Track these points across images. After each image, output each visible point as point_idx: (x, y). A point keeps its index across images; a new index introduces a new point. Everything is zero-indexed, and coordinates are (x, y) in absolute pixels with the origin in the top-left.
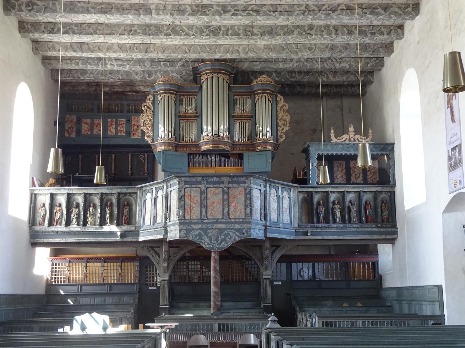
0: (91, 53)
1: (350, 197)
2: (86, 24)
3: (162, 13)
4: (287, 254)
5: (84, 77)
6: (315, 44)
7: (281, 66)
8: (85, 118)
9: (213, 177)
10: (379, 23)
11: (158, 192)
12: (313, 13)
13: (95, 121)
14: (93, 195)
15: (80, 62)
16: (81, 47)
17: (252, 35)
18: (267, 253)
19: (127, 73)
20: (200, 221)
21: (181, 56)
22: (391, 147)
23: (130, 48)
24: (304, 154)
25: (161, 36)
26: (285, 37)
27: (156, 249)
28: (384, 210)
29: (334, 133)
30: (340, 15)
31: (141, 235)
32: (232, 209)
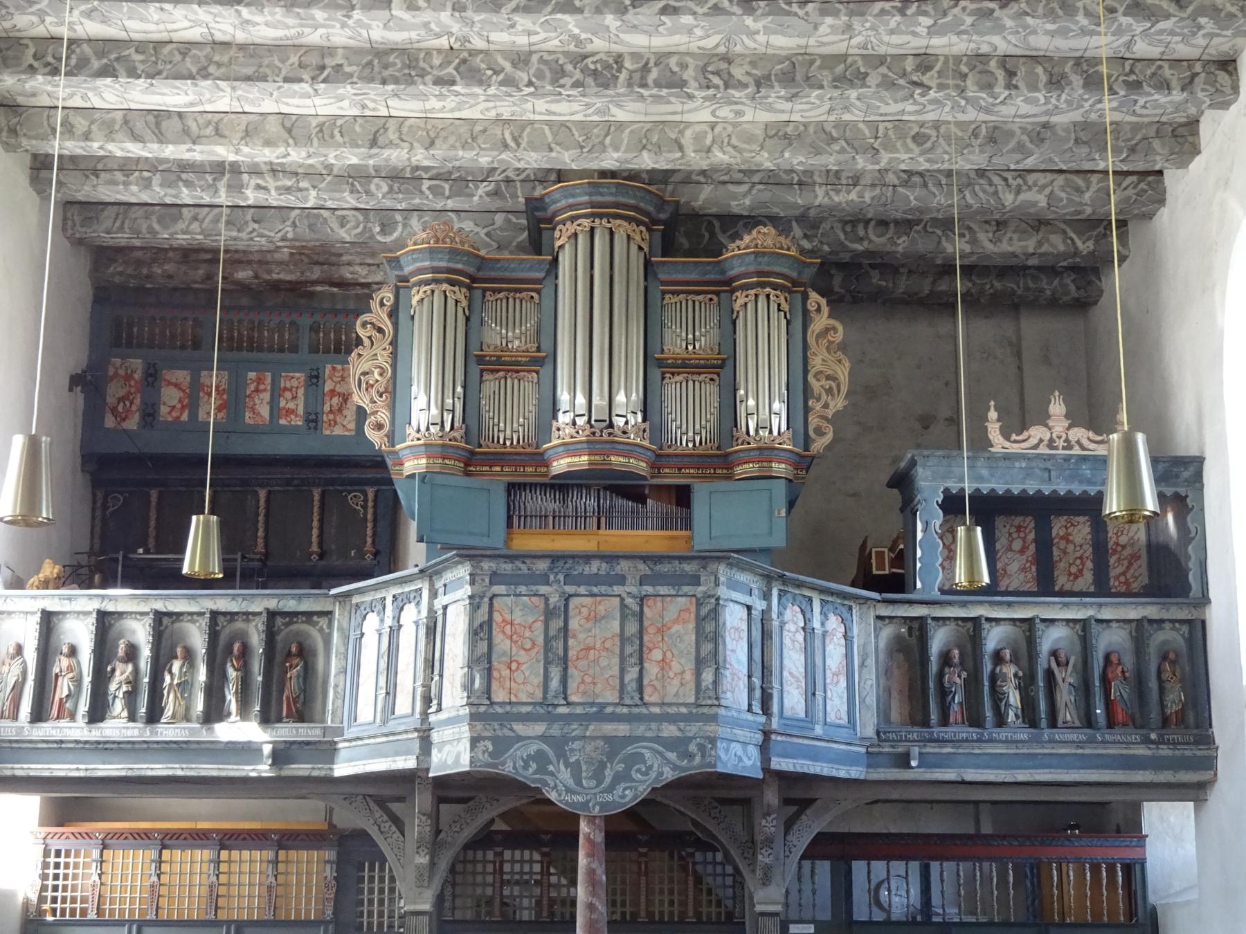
1: (1051, 638)
2: (170, 47)
3: (425, 5)
4: (833, 829)
5: (172, 230)
6: (937, 125)
7: (820, 196)
8: (171, 368)
10: (1154, 52)
11: (402, 609)
12: (935, 9)
15: (157, 180)
16: (158, 124)
17: (727, 86)
18: (769, 825)
20: (542, 711)
21: (490, 159)
22: (1192, 469)
23: (321, 131)
24: (896, 491)
25: (421, 87)
26: (836, 93)
27: (395, 807)
28: (1168, 685)
29: (998, 420)
30: (1028, 14)
31: (342, 754)
32: (652, 670)
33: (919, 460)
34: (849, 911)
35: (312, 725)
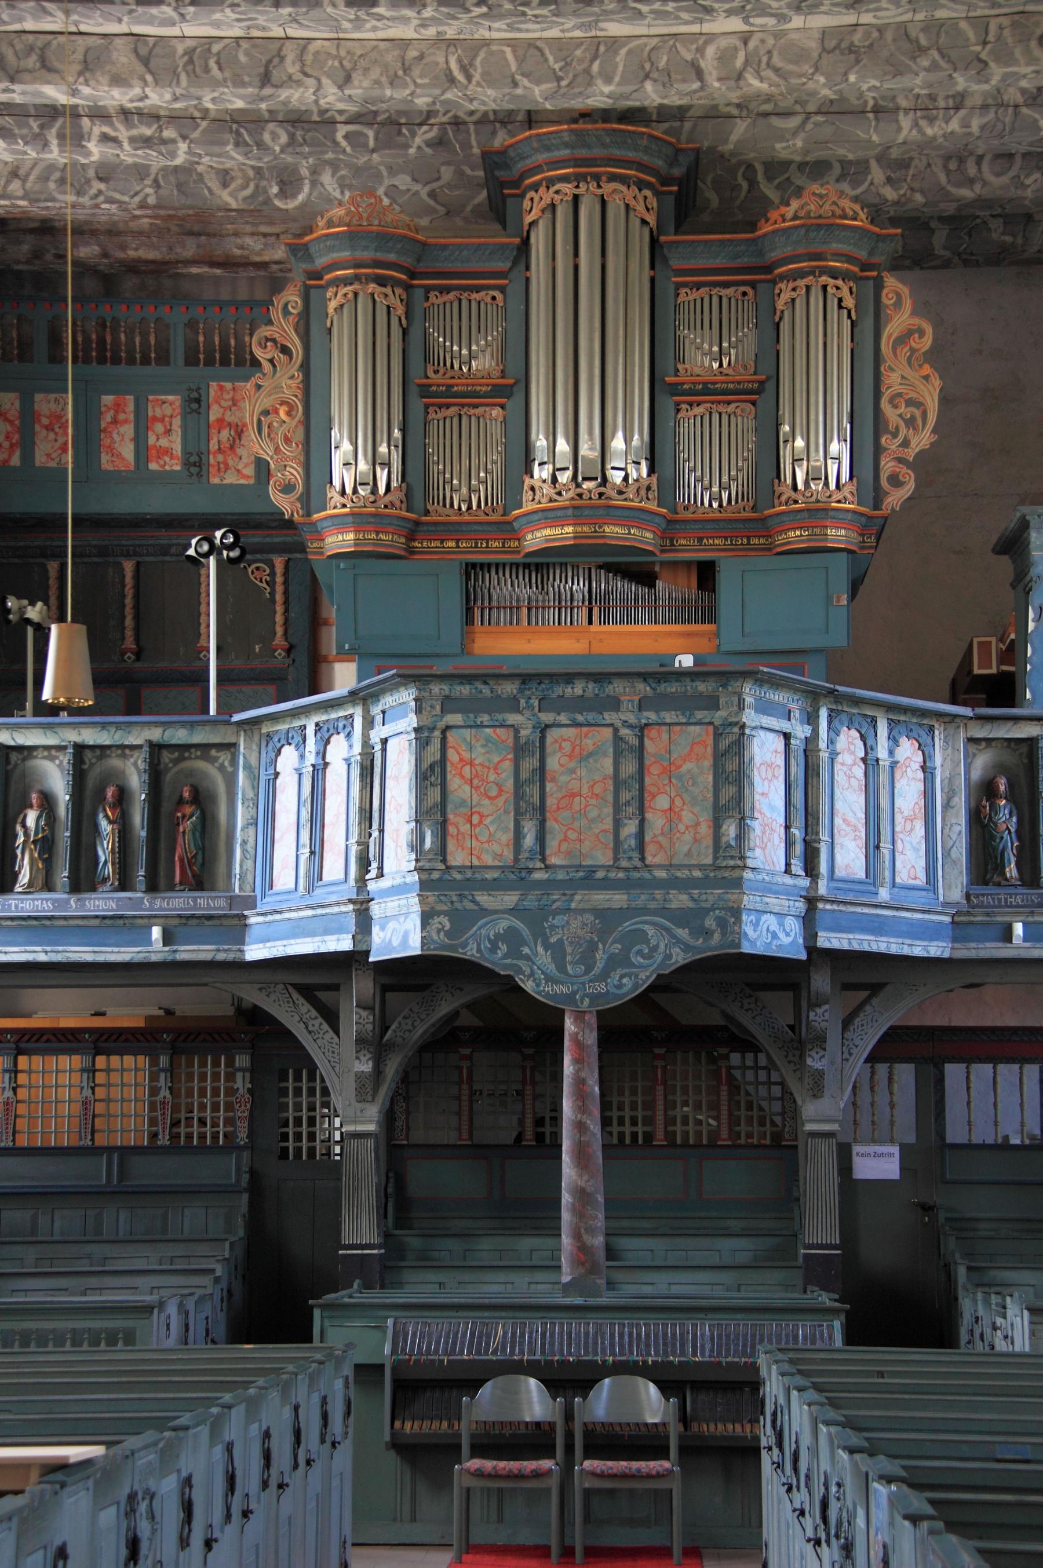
0: (7, 84)
4: (914, 1022)
9: (569, 678)
13: (43, 403)
14: (40, 753)
19: (184, 176)
21: (429, 100)
23: (191, 61)
24: (1005, 559)
31: (252, 934)
32: (656, 821)
33: (1034, 522)
34: (941, 1134)
35: (213, 894)
